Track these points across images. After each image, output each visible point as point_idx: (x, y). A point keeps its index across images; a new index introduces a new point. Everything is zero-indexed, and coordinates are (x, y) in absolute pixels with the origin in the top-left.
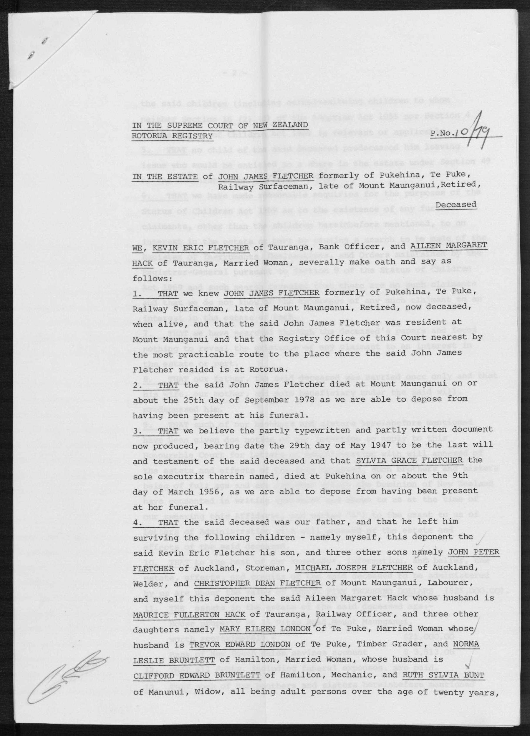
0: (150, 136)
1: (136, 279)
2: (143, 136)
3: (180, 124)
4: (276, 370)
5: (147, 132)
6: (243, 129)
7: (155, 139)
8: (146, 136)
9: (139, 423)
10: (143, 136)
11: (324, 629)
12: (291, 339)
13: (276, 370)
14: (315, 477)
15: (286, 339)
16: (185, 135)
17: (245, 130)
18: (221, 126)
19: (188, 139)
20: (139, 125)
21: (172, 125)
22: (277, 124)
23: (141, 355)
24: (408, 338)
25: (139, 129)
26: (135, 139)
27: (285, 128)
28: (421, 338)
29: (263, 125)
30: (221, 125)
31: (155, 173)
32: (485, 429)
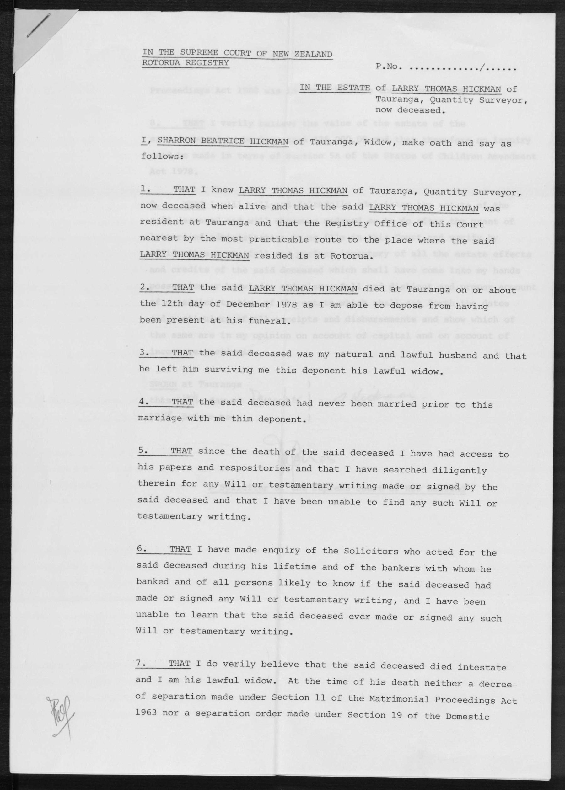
1: (145, 157)
2: (154, 63)
3: (194, 51)
8: (157, 63)
10: (154, 63)
12: (339, 224)
13: (361, 257)
15: (333, 224)
16: (199, 62)
18: (237, 53)
19: (202, 66)
21: (185, 51)
22: (300, 53)
24: (465, 225)
25: (151, 55)
26: (145, 66)
27: (308, 57)
28: (478, 226)
29: (283, 54)
30: (237, 52)
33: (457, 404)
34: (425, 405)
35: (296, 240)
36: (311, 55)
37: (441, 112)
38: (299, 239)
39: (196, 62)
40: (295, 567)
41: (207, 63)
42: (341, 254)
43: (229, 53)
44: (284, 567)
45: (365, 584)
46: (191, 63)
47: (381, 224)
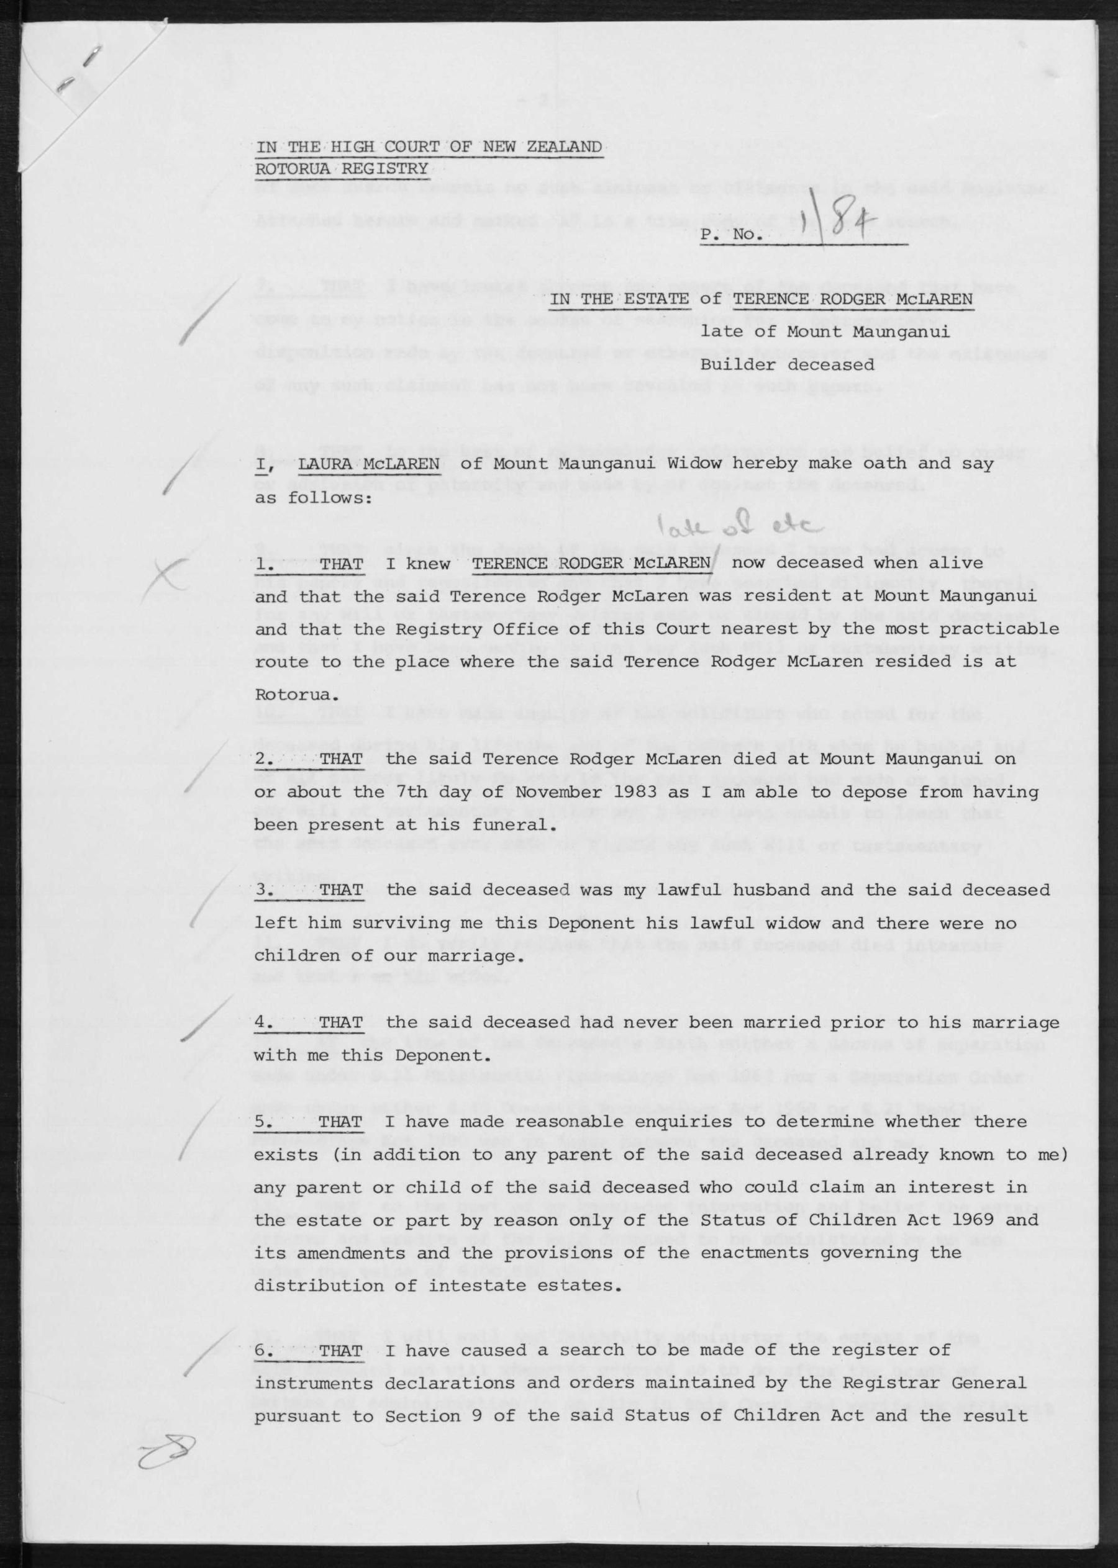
0: (293, 169)
2: (279, 170)
4: (315, 696)
5: (289, 161)
6: (460, 153)
7: (305, 176)
8: (285, 170)
10: (279, 170)
11: (642, 1254)
13: (315, 696)
14: (407, 826)
17: (465, 154)
20: (272, 146)
22: (537, 145)
24: (672, 630)
25: (272, 154)
28: (699, 630)
31: (598, 292)
32: (619, 924)
33: (1009, 1152)
34: (946, 630)
36: (559, 148)
39: (362, 168)
41: (385, 168)
42: (277, 691)
46: (352, 170)
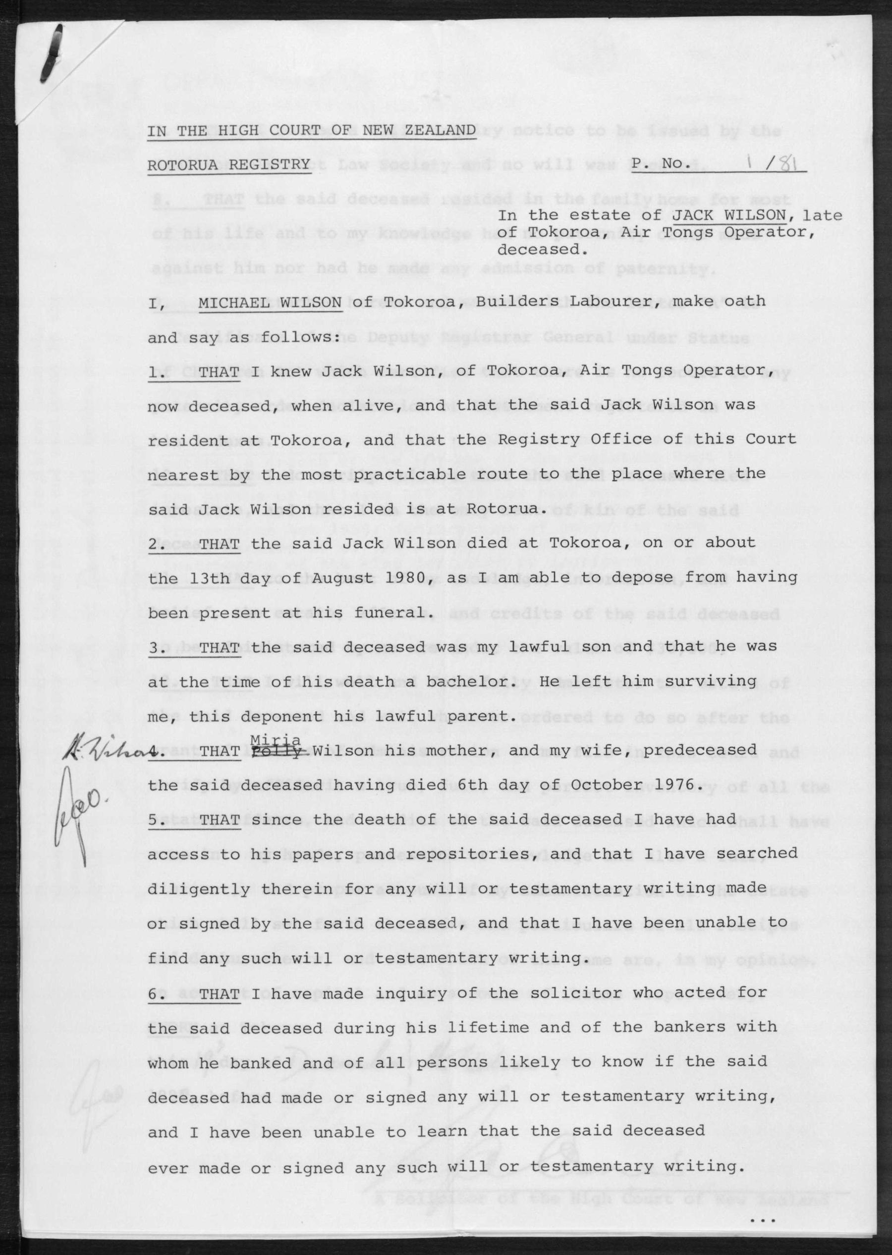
2: (169, 167)
7: (194, 171)
9: (160, 527)
10: (169, 167)
19: (259, 171)
22: (414, 129)
23: (163, 787)
26: (153, 172)
29: (382, 130)
31: (192, 125)
34: (649, 751)
35: (442, 475)
36: (435, 132)
37: (581, 251)
38: (448, 473)
40: (489, 1028)
43: (278, 130)
44: (467, 1028)
45: (664, 1062)
47: (603, 440)
